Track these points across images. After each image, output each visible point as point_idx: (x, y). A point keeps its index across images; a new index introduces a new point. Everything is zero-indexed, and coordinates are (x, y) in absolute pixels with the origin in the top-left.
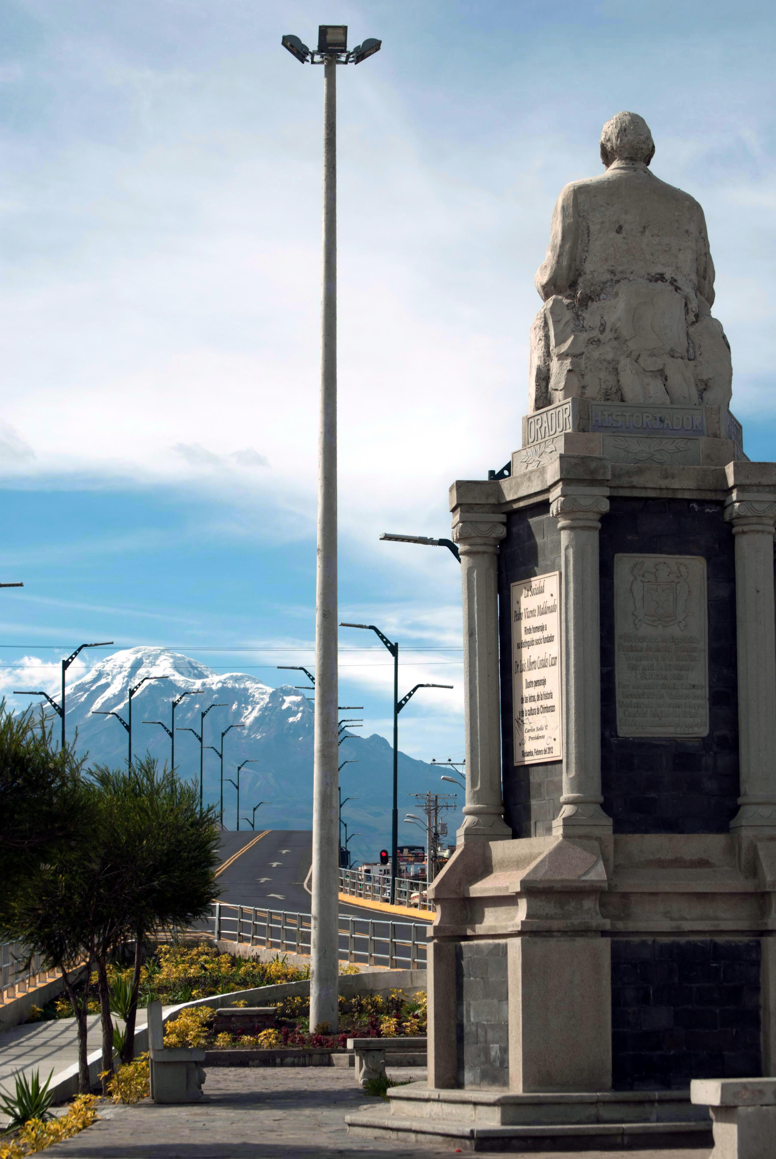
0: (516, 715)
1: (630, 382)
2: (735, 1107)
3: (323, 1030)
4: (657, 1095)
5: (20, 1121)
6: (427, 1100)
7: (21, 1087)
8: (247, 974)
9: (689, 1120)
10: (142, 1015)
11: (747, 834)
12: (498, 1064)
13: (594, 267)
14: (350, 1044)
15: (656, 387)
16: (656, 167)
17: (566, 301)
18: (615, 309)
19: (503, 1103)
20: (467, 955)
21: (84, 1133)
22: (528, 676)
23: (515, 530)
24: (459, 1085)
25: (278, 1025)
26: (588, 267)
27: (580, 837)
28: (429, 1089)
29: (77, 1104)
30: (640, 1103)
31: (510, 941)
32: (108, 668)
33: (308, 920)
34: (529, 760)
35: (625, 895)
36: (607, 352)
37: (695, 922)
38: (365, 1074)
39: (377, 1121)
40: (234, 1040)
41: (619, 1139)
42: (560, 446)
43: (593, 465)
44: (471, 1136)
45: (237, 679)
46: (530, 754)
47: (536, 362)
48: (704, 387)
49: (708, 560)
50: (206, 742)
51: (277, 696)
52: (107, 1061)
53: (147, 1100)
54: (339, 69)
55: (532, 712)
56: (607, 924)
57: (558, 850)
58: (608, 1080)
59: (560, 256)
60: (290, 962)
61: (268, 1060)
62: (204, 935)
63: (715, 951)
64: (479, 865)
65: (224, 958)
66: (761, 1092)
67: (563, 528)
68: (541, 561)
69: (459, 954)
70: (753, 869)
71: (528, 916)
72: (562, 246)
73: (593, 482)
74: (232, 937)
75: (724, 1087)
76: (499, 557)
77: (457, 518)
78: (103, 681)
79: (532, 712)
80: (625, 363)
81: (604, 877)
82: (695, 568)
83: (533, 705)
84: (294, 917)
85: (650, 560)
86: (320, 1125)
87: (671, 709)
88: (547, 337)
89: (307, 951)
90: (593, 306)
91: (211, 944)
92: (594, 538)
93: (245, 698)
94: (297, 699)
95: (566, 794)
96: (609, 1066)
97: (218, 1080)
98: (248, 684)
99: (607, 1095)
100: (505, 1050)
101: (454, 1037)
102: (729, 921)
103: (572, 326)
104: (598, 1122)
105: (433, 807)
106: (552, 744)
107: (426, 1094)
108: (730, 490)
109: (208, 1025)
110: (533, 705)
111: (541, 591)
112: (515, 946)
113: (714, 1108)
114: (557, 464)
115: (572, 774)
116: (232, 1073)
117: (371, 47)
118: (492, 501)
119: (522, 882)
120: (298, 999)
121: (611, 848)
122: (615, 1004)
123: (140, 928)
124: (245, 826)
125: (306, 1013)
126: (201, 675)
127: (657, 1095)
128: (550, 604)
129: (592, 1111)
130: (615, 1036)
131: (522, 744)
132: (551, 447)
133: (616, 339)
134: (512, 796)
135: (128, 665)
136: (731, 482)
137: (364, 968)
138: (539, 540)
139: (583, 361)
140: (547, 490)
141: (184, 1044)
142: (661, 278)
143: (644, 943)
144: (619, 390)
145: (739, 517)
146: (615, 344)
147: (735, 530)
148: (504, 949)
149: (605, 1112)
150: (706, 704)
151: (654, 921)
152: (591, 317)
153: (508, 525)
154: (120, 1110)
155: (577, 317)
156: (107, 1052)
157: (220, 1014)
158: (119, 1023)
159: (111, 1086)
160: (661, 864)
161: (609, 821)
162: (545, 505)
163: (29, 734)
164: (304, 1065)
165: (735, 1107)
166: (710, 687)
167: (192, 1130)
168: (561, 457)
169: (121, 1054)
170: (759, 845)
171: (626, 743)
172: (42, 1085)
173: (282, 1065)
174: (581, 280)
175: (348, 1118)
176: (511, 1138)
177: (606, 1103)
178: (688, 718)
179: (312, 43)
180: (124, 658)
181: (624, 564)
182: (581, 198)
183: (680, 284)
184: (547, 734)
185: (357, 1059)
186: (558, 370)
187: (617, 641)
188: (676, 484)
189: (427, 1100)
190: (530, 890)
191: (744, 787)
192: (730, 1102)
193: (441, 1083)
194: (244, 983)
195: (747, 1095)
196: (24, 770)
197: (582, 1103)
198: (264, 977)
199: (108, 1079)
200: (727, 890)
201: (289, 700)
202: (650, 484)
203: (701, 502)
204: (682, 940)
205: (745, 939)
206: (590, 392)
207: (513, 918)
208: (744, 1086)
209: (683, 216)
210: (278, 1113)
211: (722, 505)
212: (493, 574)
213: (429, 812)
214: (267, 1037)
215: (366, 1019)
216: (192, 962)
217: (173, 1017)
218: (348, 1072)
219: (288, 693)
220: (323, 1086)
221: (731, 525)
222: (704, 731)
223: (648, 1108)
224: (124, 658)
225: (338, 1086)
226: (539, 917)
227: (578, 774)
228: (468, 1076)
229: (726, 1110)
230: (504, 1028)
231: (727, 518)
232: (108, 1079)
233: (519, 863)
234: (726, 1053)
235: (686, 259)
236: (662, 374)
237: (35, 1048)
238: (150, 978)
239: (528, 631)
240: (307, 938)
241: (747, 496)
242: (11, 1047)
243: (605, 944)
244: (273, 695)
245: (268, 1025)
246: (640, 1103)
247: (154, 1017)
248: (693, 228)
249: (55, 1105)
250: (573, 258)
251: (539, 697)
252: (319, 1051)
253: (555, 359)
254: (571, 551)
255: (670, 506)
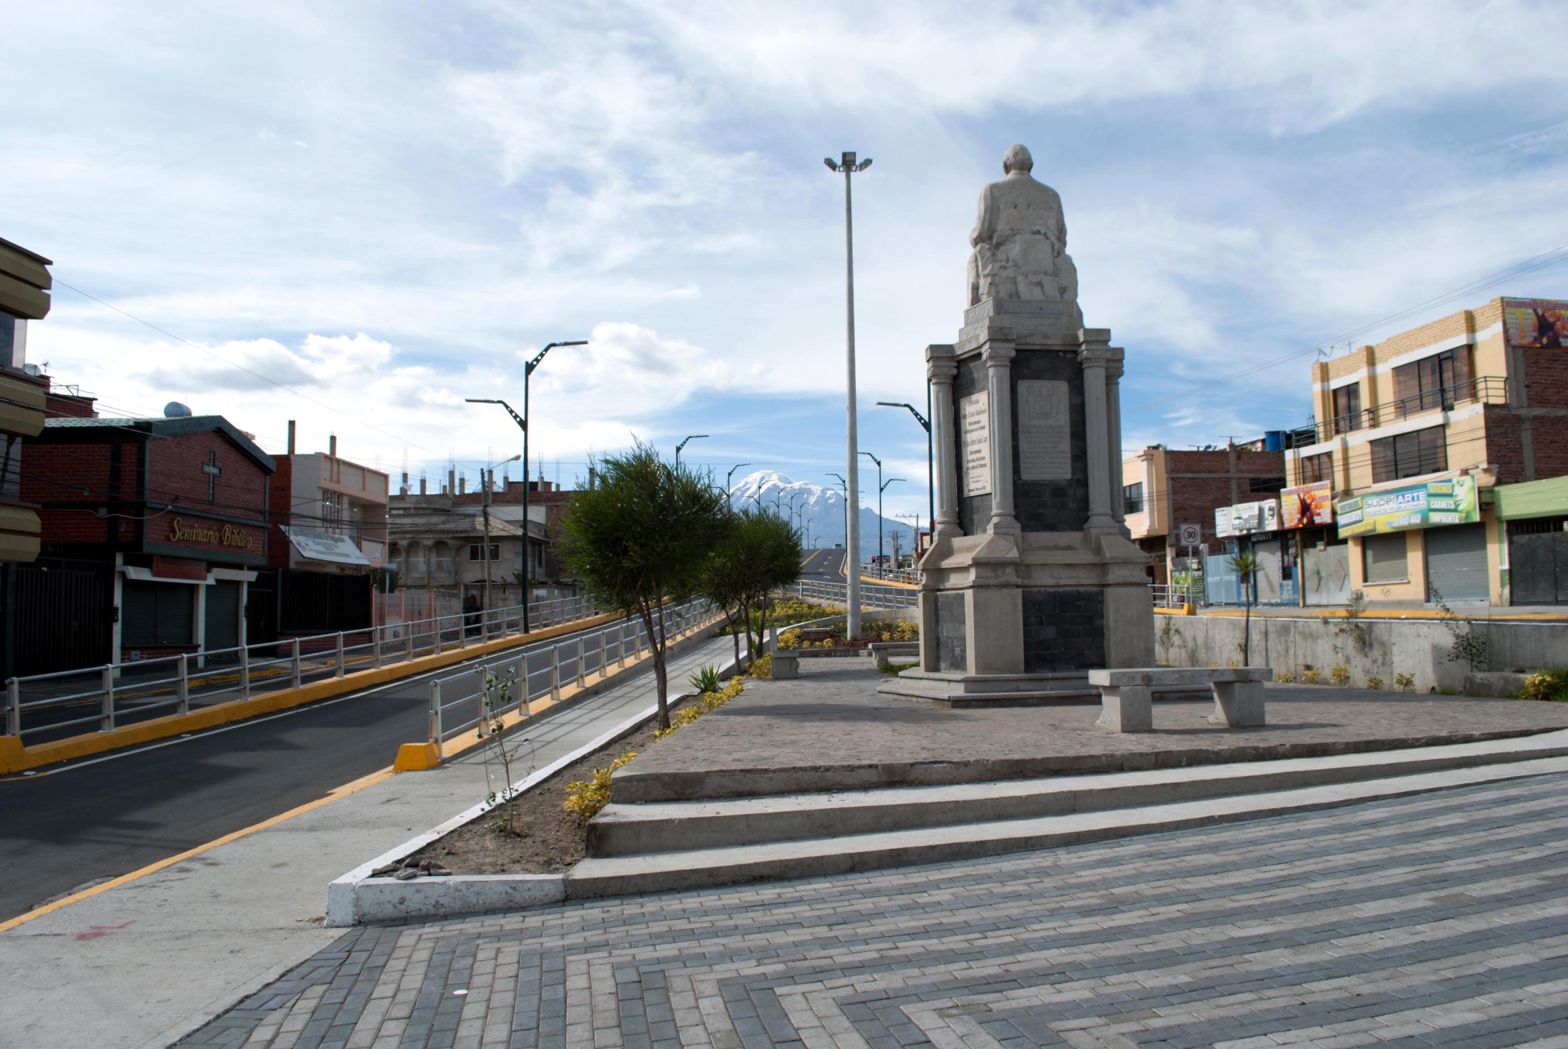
0: (964, 469)
1: (1022, 287)
2: (1118, 687)
3: (854, 638)
4: (1050, 675)
5: (704, 691)
6: (921, 679)
7: (704, 673)
8: (816, 612)
9: (1068, 689)
10: (766, 632)
11: (1094, 531)
12: (959, 658)
13: (1002, 227)
14: (870, 646)
15: (1037, 291)
16: (1035, 174)
17: (987, 247)
18: (1014, 250)
19: (965, 681)
20: (941, 599)
21: (738, 698)
22: (971, 448)
23: (962, 370)
24: (937, 669)
25: (832, 636)
26: (999, 228)
27: (1003, 534)
28: (920, 671)
29: (734, 682)
30: (1041, 680)
31: (966, 591)
32: (750, 480)
33: (845, 587)
34: (972, 494)
35: (1028, 566)
36: (1010, 272)
37: (1067, 580)
38: (879, 660)
39: (893, 690)
40: (811, 644)
41: (1031, 701)
42: (987, 323)
43: (1006, 332)
44: (949, 700)
45: (806, 484)
46: (973, 490)
47: (972, 280)
48: (1063, 291)
49: (1069, 383)
50: (794, 510)
51: (823, 491)
52: (749, 657)
53: (770, 677)
54: (852, 174)
55: (973, 468)
56: (1020, 581)
57: (992, 541)
58: (1022, 667)
59: (983, 222)
60: (835, 606)
61: (828, 654)
62: (794, 594)
63: (1079, 596)
64: (945, 551)
65: (805, 605)
66: (1133, 677)
67: (990, 366)
68: (977, 386)
69: (936, 600)
70: (1098, 551)
71: (976, 578)
72: (984, 217)
73: (1007, 340)
74: (808, 596)
75: (1112, 675)
76: (953, 386)
77: (931, 364)
78: (748, 486)
79: (973, 468)
80: (1020, 278)
81: (1017, 555)
82: (1062, 388)
83: (974, 464)
84: (837, 586)
85: (1037, 384)
86: (861, 691)
87: (1051, 465)
88: (977, 266)
89: (845, 601)
90: (1002, 248)
91: (798, 599)
92: (1007, 372)
93: (810, 492)
94: (833, 492)
95: (995, 511)
96: (1022, 659)
97: (806, 665)
98: (811, 486)
99: (1024, 675)
100: (964, 651)
101: (934, 644)
102: (1086, 579)
103: (990, 259)
104: (1018, 690)
105: (896, 537)
106: (985, 484)
107: (921, 676)
108: (1080, 345)
109: (799, 637)
110: (974, 464)
111: (977, 402)
112: (969, 595)
113: (1104, 687)
114: (986, 332)
115: (998, 500)
116: (811, 660)
117: (867, 163)
118: (949, 355)
119: (973, 559)
120: (841, 624)
121: (1020, 540)
122: (1025, 624)
123: (765, 590)
124: (811, 547)
125: (845, 630)
126: (790, 483)
127: (1050, 675)
128: (983, 409)
129: (1014, 684)
130: (1025, 643)
131: (968, 485)
132: (982, 324)
133: (1015, 266)
134: (963, 513)
135: (758, 479)
136: (1081, 339)
137: (871, 609)
138: (975, 375)
139: (997, 278)
140: (980, 347)
141: (788, 647)
142: (1038, 232)
143: (1039, 592)
144: (1017, 293)
145: (1086, 359)
146: (1014, 268)
147: (1084, 366)
148: (963, 596)
149: (1022, 685)
150: (1069, 461)
151: (1045, 580)
152: (1001, 254)
153: (958, 367)
154: (756, 683)
155: (994, 255)
156: (750, 652)
157: (804, 632)
158: (755, 637)
159: (752, 670)
160: (1047, 548)
161: (1019, 525)
162: (979, 355)
163: (702, 481)
164: (846, 656)
165: (1118, 687)
166: (1072, 452)
167: (795, 695)
168: (989, 327)
169: (757, 653)
170: (1102, 538)
171: (1026, 483)
172: (715, 672)
173: (835, 656)
174: (995, 235)
175: (878, 689)
176: (971, 700)
177: (1022, 680)
178: (1061, 470)
179: (838, 161)
180: (756, 476)
181: (1023, 386)
182: (995, 190)
183: (1049, 235)
184: (983, 478)
185: (874, 654)
186: (984, 284)
187: (1020, 428)
188: (1050, 342)
189: (921, 679)
190: (977, 563)
191: (1092, 506)
192: (1116, 683)
193: (928, 669)
194: (815, 617)
195: (1125, 679)
196: (699, 501)
197: (1009, 680)
198: (824, 614)
199: (750, 666)
200: (1085, 562)
201: (829, 493)
202: (1037, 342)
203: (1065, 352)
204: (1061, 590)
205: (1095, 589)
206: (1001, 295)
207: (967, 579)
208: (1124, 674)
209: (1050, 201)
210: (838, 684)
211: (1075, 353)
212: (950, 394)
213: (894, 539)
214: (827, 642)
215: (874, 633)
216: (790, 607)
217: (782, 633)
218: (867, 660)
219: (828, 489)
220: (857, 667)
221: (1081, 363)
222: (1069, 476)
223: (1045, 682)
224: (756, 476)
225: (865, 667)
226: (982, 578)
227: (1001, 500)
228: (943, 665)
229: (1112, 689)
230: (963, 639)
231: (1079, 359)
232: (750, 666)
233: (969, 549)
234: (1086, 652)
235: (1052, 222)
236: (1040, 284)
237: (715, 650)
238: (771, 616)
239: (970, 424)
240: (844, 595)
241: (1091, 347)
242: (544, 724)
243: (1019, 592)
244: (822, 491)
245: (829, 637)
246: (1041, 680)
247: (773, 634)
248: (1055, 207)
249: (723, 680)
250: (990, 223)
251: (978, 460)
252: (853, 648)
253: (982, 278)
254: (995, 379)
255: (1048, 353)
